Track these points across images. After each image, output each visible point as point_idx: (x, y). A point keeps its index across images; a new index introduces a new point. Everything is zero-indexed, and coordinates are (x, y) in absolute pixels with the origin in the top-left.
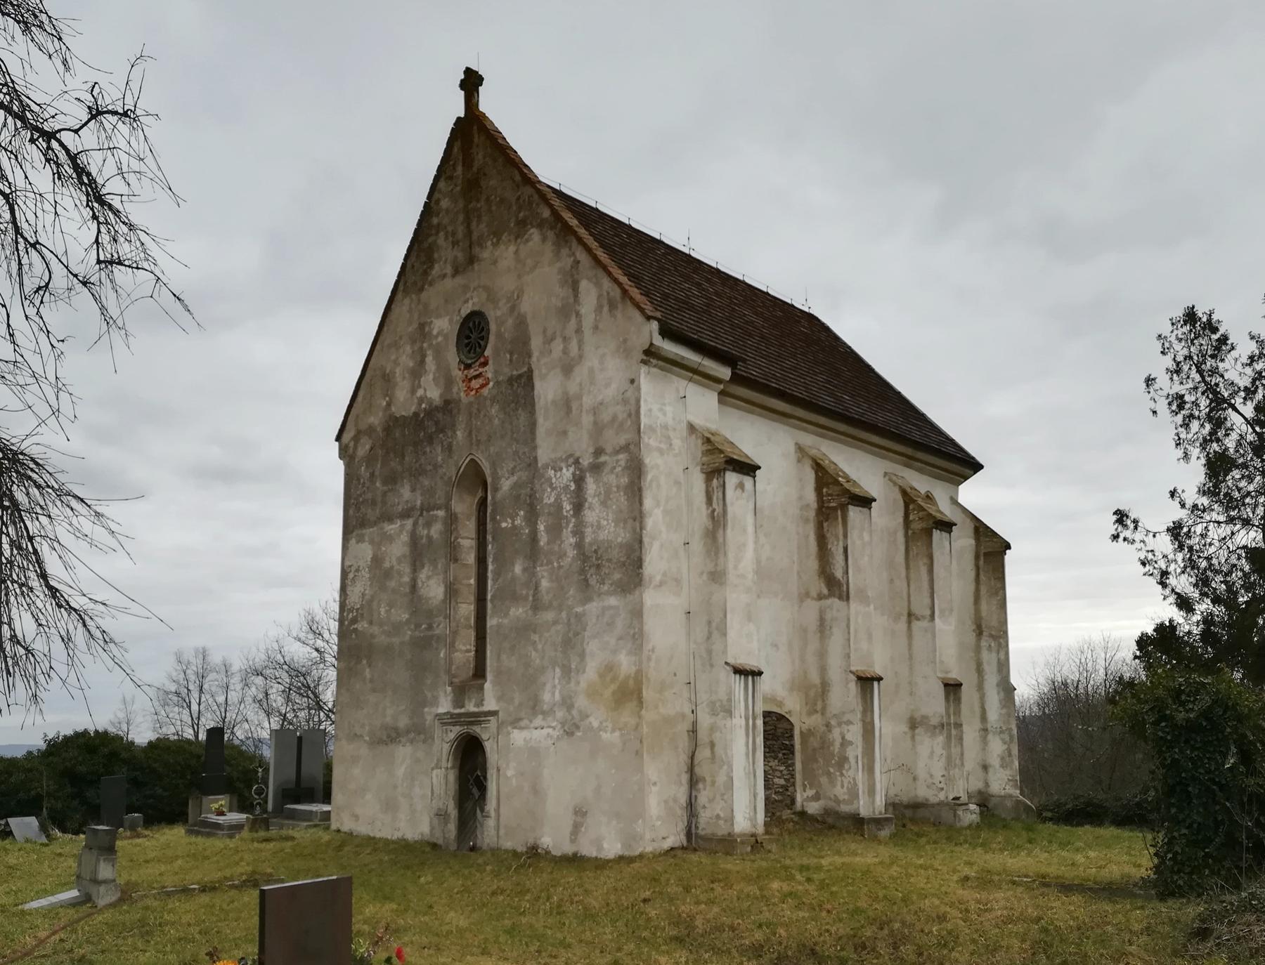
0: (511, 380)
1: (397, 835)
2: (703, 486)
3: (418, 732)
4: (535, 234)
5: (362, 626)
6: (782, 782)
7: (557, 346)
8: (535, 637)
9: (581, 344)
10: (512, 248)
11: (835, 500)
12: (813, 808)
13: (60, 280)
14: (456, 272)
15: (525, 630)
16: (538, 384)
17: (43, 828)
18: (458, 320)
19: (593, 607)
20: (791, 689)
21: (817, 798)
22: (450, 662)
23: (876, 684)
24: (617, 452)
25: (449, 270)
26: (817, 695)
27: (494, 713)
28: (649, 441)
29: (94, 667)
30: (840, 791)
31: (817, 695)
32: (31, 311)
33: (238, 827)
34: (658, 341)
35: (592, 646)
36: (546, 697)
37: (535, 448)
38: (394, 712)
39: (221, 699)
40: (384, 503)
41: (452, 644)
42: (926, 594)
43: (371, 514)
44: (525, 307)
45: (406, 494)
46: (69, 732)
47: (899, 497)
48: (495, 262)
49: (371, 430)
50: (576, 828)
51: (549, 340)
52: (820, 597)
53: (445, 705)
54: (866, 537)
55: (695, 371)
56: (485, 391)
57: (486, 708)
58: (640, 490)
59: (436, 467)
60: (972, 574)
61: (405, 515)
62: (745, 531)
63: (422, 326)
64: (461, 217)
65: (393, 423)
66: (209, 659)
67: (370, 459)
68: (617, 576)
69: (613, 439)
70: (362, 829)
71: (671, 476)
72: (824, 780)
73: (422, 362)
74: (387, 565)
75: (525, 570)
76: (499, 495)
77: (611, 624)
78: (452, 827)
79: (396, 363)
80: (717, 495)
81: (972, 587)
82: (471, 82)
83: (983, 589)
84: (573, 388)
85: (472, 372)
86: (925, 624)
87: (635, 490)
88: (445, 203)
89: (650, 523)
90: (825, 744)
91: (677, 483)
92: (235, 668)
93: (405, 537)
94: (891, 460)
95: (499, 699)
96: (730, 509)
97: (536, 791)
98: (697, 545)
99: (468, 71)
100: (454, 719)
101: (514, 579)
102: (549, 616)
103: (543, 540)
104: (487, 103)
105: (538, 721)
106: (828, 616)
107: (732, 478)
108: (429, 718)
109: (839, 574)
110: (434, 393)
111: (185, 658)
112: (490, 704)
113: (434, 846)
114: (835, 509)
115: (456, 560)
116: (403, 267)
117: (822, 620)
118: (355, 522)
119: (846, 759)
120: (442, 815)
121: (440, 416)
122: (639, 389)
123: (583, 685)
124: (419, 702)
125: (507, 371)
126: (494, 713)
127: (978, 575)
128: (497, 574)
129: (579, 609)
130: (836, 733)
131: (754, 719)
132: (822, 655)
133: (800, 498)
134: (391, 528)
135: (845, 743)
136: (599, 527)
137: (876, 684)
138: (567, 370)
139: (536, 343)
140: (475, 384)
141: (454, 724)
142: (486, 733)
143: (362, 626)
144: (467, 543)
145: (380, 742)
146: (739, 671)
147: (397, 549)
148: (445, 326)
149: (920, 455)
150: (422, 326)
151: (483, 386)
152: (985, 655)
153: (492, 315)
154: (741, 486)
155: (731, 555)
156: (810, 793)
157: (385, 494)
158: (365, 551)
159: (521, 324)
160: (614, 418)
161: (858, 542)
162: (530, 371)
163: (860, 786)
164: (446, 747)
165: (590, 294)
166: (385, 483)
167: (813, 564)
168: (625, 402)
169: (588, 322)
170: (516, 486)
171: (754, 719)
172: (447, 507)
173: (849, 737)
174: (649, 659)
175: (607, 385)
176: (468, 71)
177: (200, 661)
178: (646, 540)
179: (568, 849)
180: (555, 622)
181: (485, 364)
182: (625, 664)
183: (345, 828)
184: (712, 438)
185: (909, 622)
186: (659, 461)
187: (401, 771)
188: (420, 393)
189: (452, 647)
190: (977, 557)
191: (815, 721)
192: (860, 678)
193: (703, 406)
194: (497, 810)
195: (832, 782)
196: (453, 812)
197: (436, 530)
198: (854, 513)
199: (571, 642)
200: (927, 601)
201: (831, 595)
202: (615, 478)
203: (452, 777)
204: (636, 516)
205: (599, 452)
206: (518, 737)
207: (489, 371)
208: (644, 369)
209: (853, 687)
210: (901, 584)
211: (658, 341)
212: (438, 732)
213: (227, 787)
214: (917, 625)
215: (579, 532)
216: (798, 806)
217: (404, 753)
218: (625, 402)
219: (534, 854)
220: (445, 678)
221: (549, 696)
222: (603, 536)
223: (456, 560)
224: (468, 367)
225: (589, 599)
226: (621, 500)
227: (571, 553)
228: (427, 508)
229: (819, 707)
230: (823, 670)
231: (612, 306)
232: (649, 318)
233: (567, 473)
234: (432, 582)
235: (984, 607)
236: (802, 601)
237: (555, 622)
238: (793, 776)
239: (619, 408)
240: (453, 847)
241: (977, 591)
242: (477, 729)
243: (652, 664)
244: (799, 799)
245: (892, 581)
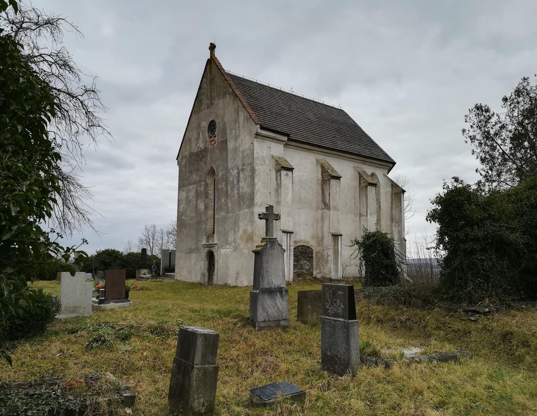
0: (222, 142)
2: (275, 175)
4: (228, 97)
5: (183, 217)
6: (308, 267)
8: (227, 221)
9: (239, 131)
10: (222, 101)
11: (328, 177)
12: (319, 276)
14: (208, 108)
15: (225, 219)
16: (228, 143)
17: (93, 276)
18: (208, 123)
19: (241, 212)
20: (313, 239)
21: (320, 273)
23: (340, 237)
24: (248, 165)
25: (206, 107)
29: (85, 226)
30: (326, 271)
31: (320, 241)
32: (74, 138)
33: (148, 278)
34: (260, 131)
35: (241, 224)
36: (230, 239)
37: (227, 163)
39: (160, 242)
40: (189, 179)
42: (365, 207)
43: (186, 183)
44: (225, 119)
45: (195, 177)
46: (104, 249)
48: (218, 105)
49: (186, 157)
50: (236, 279)
51: (231, 130)
52: (322, 209)
53: (204, 242)
54: (338, 189)
56: (215, 145)
58: (254, 177)
60: (390, 201)
61: (194, 183)
62: (288, 189)
63: (199, 124)
65: (192, 154)
67: (185, 166)
68: (248, 203)
70: (183, 279)
71: (264, 172)
72: (322, 267)
74: (190, 199)
76: (218, 178)
78: (206, 279)
79: (192, 136)
80: (279, 178)
82: (212, 47)
84: (237, 145)
85: (212, 139)
86: (364, 218)
87: (252, 177)
88: (205, 86)
89: (257, 187)
90: (322, 256)
91: (267, 174)
92: (164, 232)
93: (194, 190)
95: (218, 240)
96: (282, 182)
97: (227, 267)
98: (273, 193)
99: (211, 44)
100: (206, 246)
101: (222, 203)
102: (231, 215)
104: (218, 54)
105: (228, 247)
106: (324, 215)
107: (283, 173)
108: (200, 246)
109: (327, 201)
110: (202, 146)
112: (216, 242)
113: (201, 284)
114: (326, 180)
115: (207, 197)
116: (194, 105)
117: (322, 216)
118: (181, 186)
119: (328, 260)
120: (203, 275)
121: (203, 152)
122: (254, 146)
123: (239, 236)
127: (392, 201)
128: (218, 202)
129: (238, 213)
130: (326, 252)
131: (290, 246)
132: (322, 228)
133: (317, 177)
134: (191, 187)
135: (328, 255)
136: (243, 188)
137: (340, 237)
138: (236, 139)
139: (228, 130)
140: (213, 143)
141: (207, 247)
143: (183, 217)
144: (211, 192)
145: (188, 253)
146: (283, 232)
147: (192, 194)
148: (205, 125)
149: (368, 160)
150: (199, 124)
151: (215, 143)
152: (394, 228)
153: (217, 121)
154: (287, 175)
155: (283, 196)
156: (318, 271)
157: (189, 177)
158: (184, 194)
159: (224, 124)
160: (248, 154)
161: (334, 191)
162: (227, 139)
163: (332, 269)
164: (205, 254)
165: (242, 116)
166: (189, 173)
167: (320, 198)
168: (250, 149)
170: (223, 175)
171: (290, 246)
173: (329, 254)
174: (256, 228)
175: (246, 144)
176: (211, 44)
177: (153, 229)
179: (235, 285)
180: (232, 217)
181: (215, 137)
182: (249, 229)
183: (178, 279)
185: (360, 217)
186: (261, 168)
187: (193, 262)
188: (198, 145)
189: (206, 224)
191: (319, 249)
192: (333, 235)
193: (277, 150)
194: (217, 273)
195: (324, 268)
197: (202, 188)
198: (333, 182)
199: (236, 223)
200: (365, 210)
201: (325, 208)
202: (248, 173)
203: (206, 263)
205: (243, 165)
206: (223, 251)
207: (216, 139)
208: (256, 139)
209: (331, 237)
210: (358, 204)
211: (260, 131)
212: (202, 250)
214: (362, 218)
215: (238, 190)
216: (314, 275)
217: (194, 256)
218: (250, 149)
219: (226, 286)
220: (204, 233)
221: (231, 239)
222: (244, 190)
223: (207, 197)
224: (211, 137)
225: (240, 210)
226: (249, 180)
227: (236, 196)
228: (200, 181)
229: (321, 244)
230: (322, 232)
232: (256, 124)
233: (236, 171)
235: (394, 212)
236: (317, 210)
238: (312, 266)
239: (249, 151)
240: (207, 284)
241: (392, 206)
242: (212, 249)
243: (257, 229)
244: (314, 273)
245: (355, 203)
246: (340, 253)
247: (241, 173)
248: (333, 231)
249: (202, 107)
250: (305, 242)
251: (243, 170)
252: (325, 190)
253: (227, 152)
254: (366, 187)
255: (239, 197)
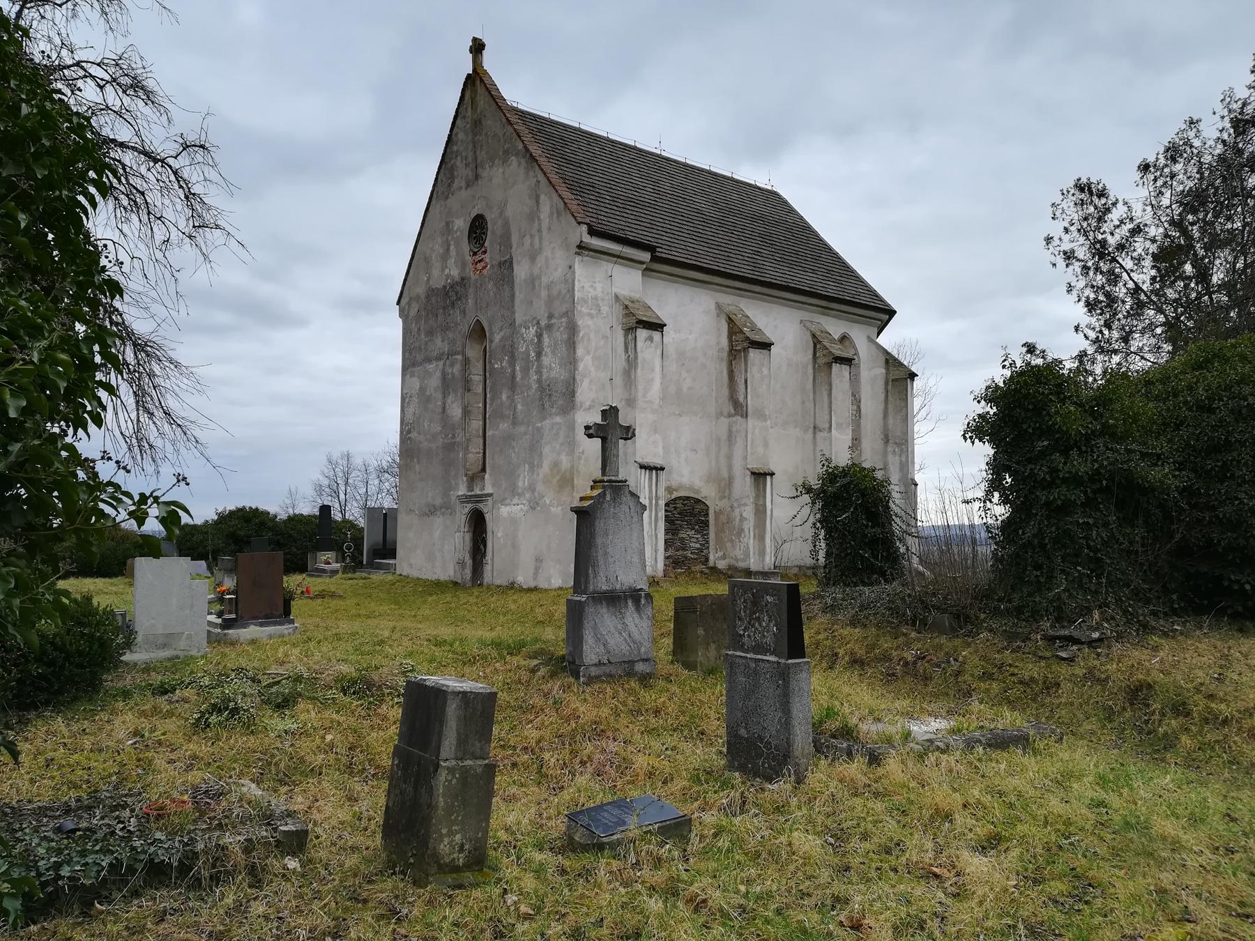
0: (500, 264)
1: (434, 577)
3: (446, 508)
5: (414, 435)
6: (698, 546)
7: (527, 241)
8: (514, 444)
9: (541, 238)
11: (744, 343)
12: (722, 565)
13: (175, 235)
15: (509, 438)
17: (210, 568)
18: (469, 220)
19: (547, 422)
21: (724, 557)
22: (465, 460)
23: (768, 478)
24: (561, 317)
25: (463, 184)
26: (726, 485)
27: (491, 495)
28: (582, 309)
30: (738, 553)
33: (335, 572)
34: (587, 239)
35: (546, 450)
36: (520, 484)
37: (514, 313)
38: (433, 495)
41: (467, 448)
42: (827, 412)
43: (419, 357)
44: (509, 212)
46: (233, 508)
47: (810, 338)
49: (418, 298)
50: (536, 573)
52: (730, 416)
53: (462, 490)
54: (765, 371)
55: (619, 257)
56: (485, 272)
57: (486, 492)
59: (456, 324)
60: (882, 397)
61: (438, 358)
62: (653, 370)
64: (471, 146)
66: (352, 460)
67: (418, 318)
68: (561, 402)
69: (560, 308)
70: (415, 573)
71: (598, 334)
72: (729, 545)
73: (448, 249)
75: (508, 397)
76: (493, 345)
77: (557, 434)
78: (468, 572)
80: (631, 346)
81: (882, 407)
82: (477, 48)
83: (890, 407)
84: (536, 271)
85: (477, 258)
86: (825, 434)
87: (571, 344)
88: (461, 136)
89: (581, 366)
90: (729, 520)
91: (605, 337)
92: (371, 469)
93: (438, 374)
94: (806, 310)
95: (493, 485)
97: (515, 546)
98: (619, 381)
99: (475, 39)
100: (466, 499)
102: (522, 429)
103: (519, 376)
105: (515, 501)
106: (734, 430)
107: (642, 334)
108: (453, 498)
109: (741, 399)
110: (455, 273)
111: (334, 458)
112: (489, 489)
113: (456, 583)
117: (730, 431)
119: (743, 530)
120: (461, 564)
124: (447, 489)
125: (498, 258)
126: (490, 495)
127: (887, 397)
128: (492, 400)
130: (737, 512)
132: (729, 457)
134: (430, 367)
135: (742, 519)
136: (551, 368)
137: (768, 478)
139: (515, 239)
140: (480, 266)
141: (468, 502)
142: (485, 508)
143: (414, 435)
144: (477, 378)
146: (642, 467)
147: (434, 382)
148: (461, 224)
150: (447, 224)
154: (651, 339)
156: (720, 554)
157: (426, 344)
158: (415, 383)
159: (506, 225)
160: (560, 293)
161: (757, 376)
162: (511, 258)
165: (547, 204)
166: (426, 335)
167: (725, 391)
169: (545, 222)
171: (657, 498)
172: (463, 354)
174: (580, 458)
175: (556, 269)
178: (578, 377)
179: (532, 585)
180: (526, 433)
181: (485, 252)
182: (565, 461)
184: (630, 305)
186: (590, 323)
188: (447, 271)
190: (886, 383)
191: (723, 504)
192: (753, 473)
193: (628, 281)
196: (469, 562)
197: (457, 369)
198: (754, 354)
199: (534, 448)
200: (827, 417)
202: (560, 335)
203: (468, 537)
204: (571, 362)
205: (550, 317)
206: (504, 511)
207: (487, 257)
208: (578, 258)
209: (749, 479)
210: (810, 405)
211: (587, 239)
213: (336, 546)
214: (820, 435)
215: (539, 372)
216: (711, 564)
217: (438, 521)
218: (566, 281)
219: (512, 586)
220: (462, 471)
221: (523, 483)
222: (553, 374)
223: (469, 390)
224: (475, 254)
225: (544, 418)
226: (563, 349)
227: (535, 386)
228: (451, 354)
230: (730, 467)
231: (559, 214)
232: (579, 223)
233: (533, 331)
234: (455, 405)
235: (891, 421)
237: (526, 433)
241: (886, 408)
242: (481, 506)
244: (711, 557)
245: (803, 403)
246: (769, 513)
247: (545, 336)
248: (755, 465)
249: (455, 185)
250: (691, 489)
251: (549, 327)
252: (737, 373)
253: (512, 288)
254: (829, 365)
255: (541, 389)
